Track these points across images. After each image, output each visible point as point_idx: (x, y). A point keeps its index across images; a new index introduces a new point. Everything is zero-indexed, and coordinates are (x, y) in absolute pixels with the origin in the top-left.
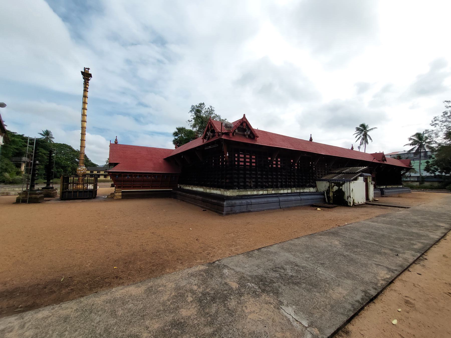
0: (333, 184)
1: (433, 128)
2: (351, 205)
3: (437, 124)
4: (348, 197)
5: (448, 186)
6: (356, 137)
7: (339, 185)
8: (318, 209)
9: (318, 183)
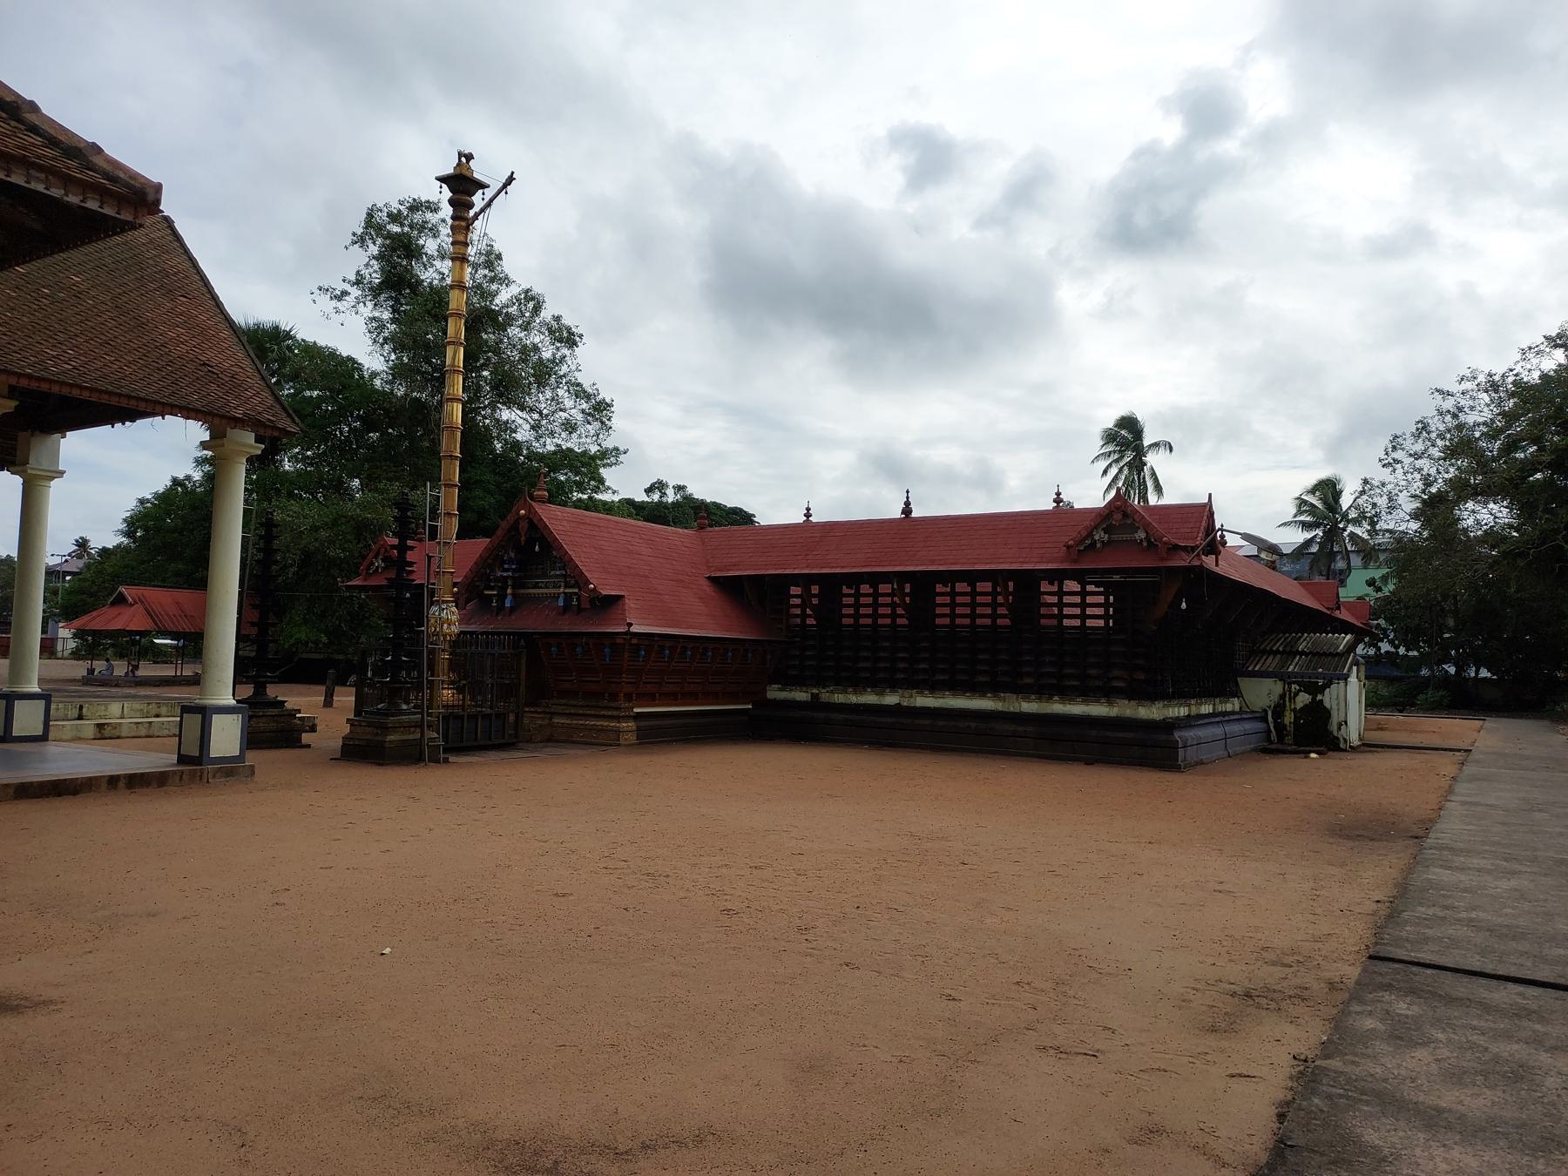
0: (1294, 687)
1: (1384, 475)
2: (1354, 738)
3: (1397, 461)
4: (1340, 725)
5: (1421, 697)
6: (1105, 472)
7: (1314, 689)
8: (1313, 755)
9: (1245, 684)
